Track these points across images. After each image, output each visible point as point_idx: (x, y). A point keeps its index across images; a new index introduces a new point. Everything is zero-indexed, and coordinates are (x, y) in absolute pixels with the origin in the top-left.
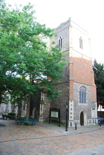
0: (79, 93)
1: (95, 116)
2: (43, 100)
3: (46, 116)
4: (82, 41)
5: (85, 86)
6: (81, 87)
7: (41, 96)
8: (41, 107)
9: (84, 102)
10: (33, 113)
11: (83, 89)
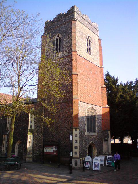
1: (108, 150)
2: (33, 128)
3: (37, 153)
4: (90, 42)
5: (94, 107)
9: (93, 131)
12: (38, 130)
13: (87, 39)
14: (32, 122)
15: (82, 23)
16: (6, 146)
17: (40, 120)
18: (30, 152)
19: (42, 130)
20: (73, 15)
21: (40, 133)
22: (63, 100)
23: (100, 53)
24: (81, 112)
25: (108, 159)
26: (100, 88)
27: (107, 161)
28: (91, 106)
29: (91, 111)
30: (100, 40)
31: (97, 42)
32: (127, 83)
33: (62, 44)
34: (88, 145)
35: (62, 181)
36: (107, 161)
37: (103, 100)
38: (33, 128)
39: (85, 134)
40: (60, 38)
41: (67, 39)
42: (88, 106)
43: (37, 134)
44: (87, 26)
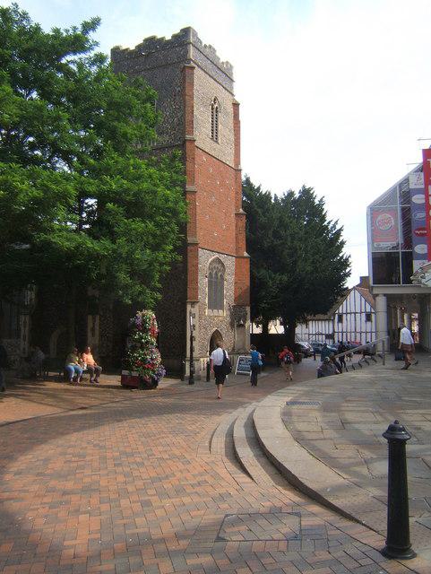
1: (244, 344)
4: (217, 112)
5: (222, 257)
6: (213, 261)
8: (90, 325)
13: (212, 106)
20: (187, 52)
26: (190, 387)
28: (217, 255)
31: (231, 110)
34: (210, 334)
35: (165, 417)
37: (237, 242)
44: (213, 73)
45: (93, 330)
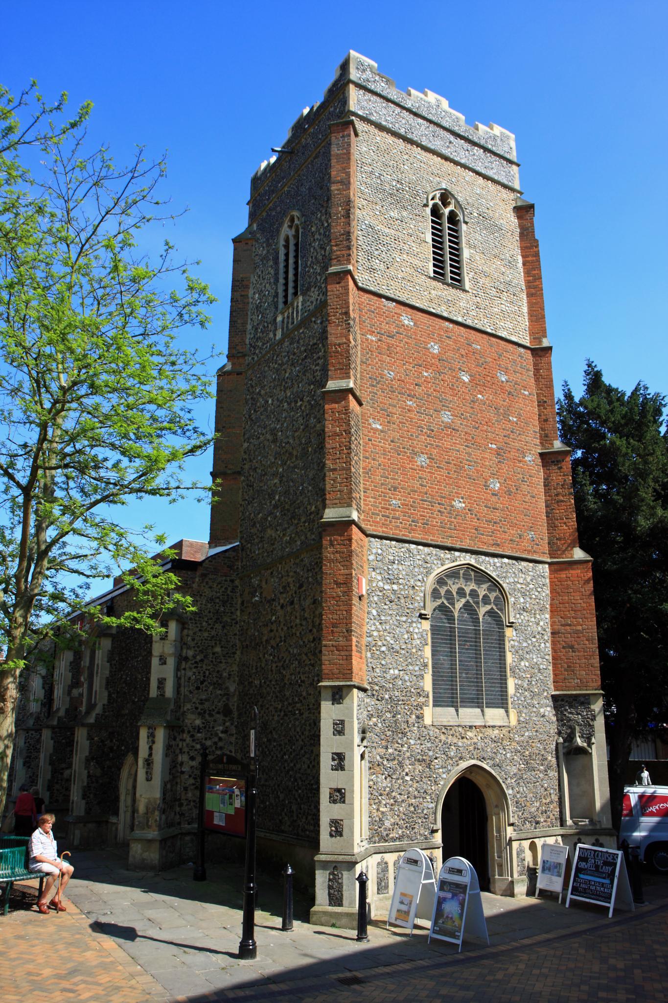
0: (426, 625)
5: (488, 565)
7: (155, 661)
10: (122, 798)
11: (473, 593)
12: (206, 700)
14: (165, 663)
15: (402, 131)
16: (85, 780)
17: (218, 649)
18: (148, 812)
19: (234, 703)
21: (220, 717)
22: (303, 538)
23: (527, 273)
24: (389, 593)
25: (583, 865)
26: (531, 458)
27: (576, 876)
29: (468, 590)
30: (524, 211)
31: (511, 221)
32: (637, 389)
33: (302, 257)
36: (617, 873)
37: (552, 525)
38: (169, 691)
39: (420, 717)
40: (297, 231)
41: (323, 225)
42: (439, 559)
43: (198, 722)
45: (149, 763)
